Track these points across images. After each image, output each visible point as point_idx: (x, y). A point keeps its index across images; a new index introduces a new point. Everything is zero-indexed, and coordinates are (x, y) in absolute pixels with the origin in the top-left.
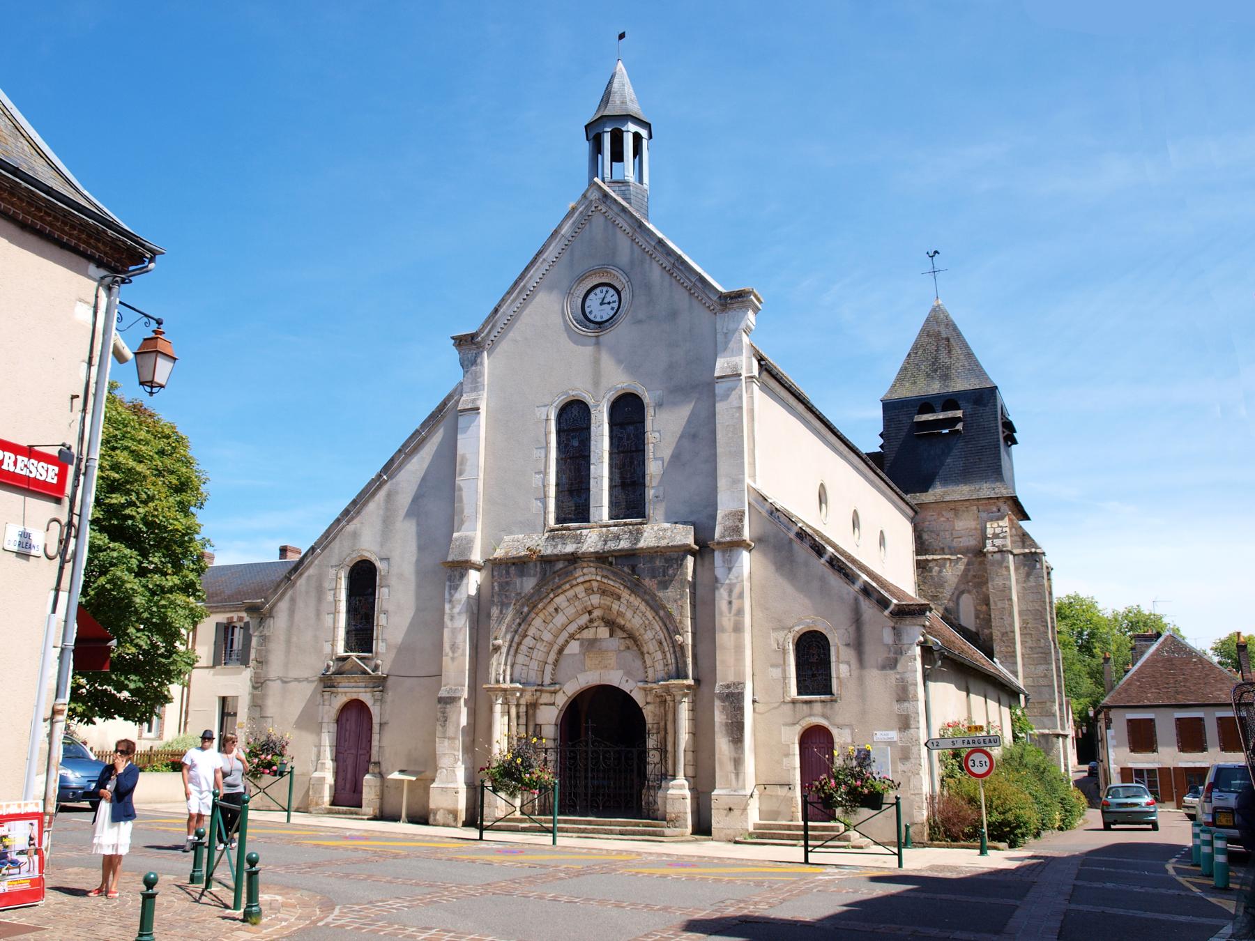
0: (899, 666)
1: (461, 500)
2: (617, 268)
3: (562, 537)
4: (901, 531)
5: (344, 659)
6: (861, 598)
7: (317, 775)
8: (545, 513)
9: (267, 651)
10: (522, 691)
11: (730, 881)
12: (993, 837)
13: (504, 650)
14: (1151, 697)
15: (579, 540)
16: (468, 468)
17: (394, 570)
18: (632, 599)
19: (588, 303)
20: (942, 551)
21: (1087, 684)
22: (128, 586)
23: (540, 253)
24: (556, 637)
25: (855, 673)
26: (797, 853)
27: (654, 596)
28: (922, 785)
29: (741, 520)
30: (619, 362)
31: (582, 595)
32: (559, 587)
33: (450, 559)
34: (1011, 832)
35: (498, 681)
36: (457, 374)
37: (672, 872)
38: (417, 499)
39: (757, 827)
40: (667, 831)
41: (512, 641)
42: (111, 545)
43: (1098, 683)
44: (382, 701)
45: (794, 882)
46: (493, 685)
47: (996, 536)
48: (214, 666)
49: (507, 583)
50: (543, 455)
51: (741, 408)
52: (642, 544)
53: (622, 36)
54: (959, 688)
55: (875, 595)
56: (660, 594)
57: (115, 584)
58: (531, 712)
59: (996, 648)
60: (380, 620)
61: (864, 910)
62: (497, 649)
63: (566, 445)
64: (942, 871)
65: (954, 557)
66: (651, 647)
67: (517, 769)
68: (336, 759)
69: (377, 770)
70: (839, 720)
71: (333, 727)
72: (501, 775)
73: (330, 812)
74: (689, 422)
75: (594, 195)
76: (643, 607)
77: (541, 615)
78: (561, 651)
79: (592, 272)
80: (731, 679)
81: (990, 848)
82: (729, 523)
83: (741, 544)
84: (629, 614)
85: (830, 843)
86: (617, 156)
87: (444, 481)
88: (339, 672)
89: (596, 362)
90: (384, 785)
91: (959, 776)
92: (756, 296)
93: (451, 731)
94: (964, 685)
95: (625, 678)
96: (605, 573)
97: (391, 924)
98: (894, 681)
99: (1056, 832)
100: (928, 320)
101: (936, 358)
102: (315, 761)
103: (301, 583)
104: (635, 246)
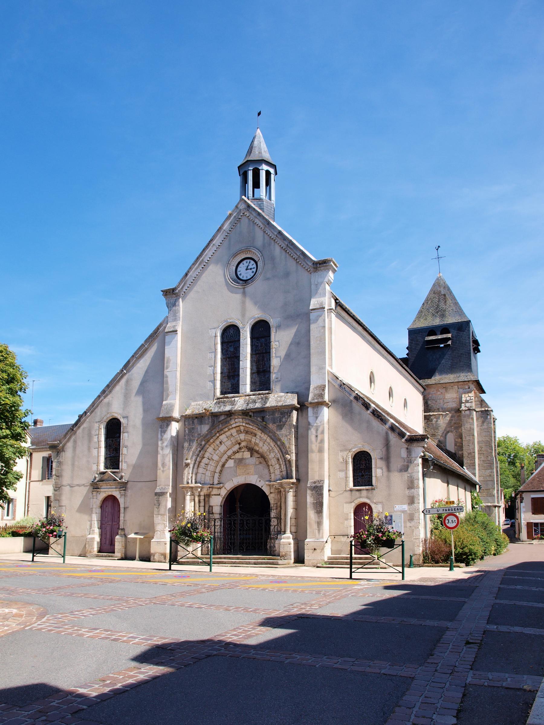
0: (409, 469)
1: (167, 383)
2: (256, 250)
3: (224, 402)
4: (416, 399)
5: (103, 473)
7: (90, 536)
8: (215, 389)
9: (62, 470)
10: (202, 488)
11: (302, 591)
12: (457, 561)
13: (191, 466)
15: (233, 403)
16: (171, 364)
17: (131, 423)
18: (263, 435)
19: (239, 269)
20: (438, 410)
21: (512, 481)
23: (211, 240)
24: (221, 457)
25: (385, 474)
26: (345, 573)
28: (419, 533)
29: (324, 390)
30: (256, 303)
31: (235, 434)
32: (222, 430)
33: (161, 416)
34: (467, 557)
35: (188, 483)
37: (270, 586)
38: (143, 383)
39: (330, 558)
44: (125, 495)
45: (340, 591)
46: (185, 485)
47: (467, 401)
48: (42, 480)
49: (193, 428)
50: (213, 356)
51: (324, 327)
52: (268, 405)
53: (259, 114)
54: (443, 482)
55: (397, 431)
58: (207, 499)
59: (465, 461)
60: (124, 451)
61: (376, 608)
62: (187, 465)
63: (227, 351)
64: (426, 581)
65: (444, 413)
66: (273, 462)
67: (189, 530)
68: (101, 528)
69: (123, 533)
71: (99, 511)
72: (180, 534)
73: (97, 556)
74: (295, 335)
75: (242, 206)
76: (268, 440)
77: (212, 445)
78: (223, 466)
79: (241, 251)
80: (317, 478)
81: (455, 566)
82: (317, 392)
84: (261, 444)
86: (256, 185)
88: (101, 480)
89: (243, 303)
90: (127, 542)
91: (441, 528)
92: (334, 263)
93: (162, 510)
94: (446, 480)
95: (259, 480)
96: (247, 422)
97: (73, 627)
98: (406, 477)
99: (492, 556)
101: (438, 306)
102: (85, 527)
103: (80, 432)
104: (266, 236)
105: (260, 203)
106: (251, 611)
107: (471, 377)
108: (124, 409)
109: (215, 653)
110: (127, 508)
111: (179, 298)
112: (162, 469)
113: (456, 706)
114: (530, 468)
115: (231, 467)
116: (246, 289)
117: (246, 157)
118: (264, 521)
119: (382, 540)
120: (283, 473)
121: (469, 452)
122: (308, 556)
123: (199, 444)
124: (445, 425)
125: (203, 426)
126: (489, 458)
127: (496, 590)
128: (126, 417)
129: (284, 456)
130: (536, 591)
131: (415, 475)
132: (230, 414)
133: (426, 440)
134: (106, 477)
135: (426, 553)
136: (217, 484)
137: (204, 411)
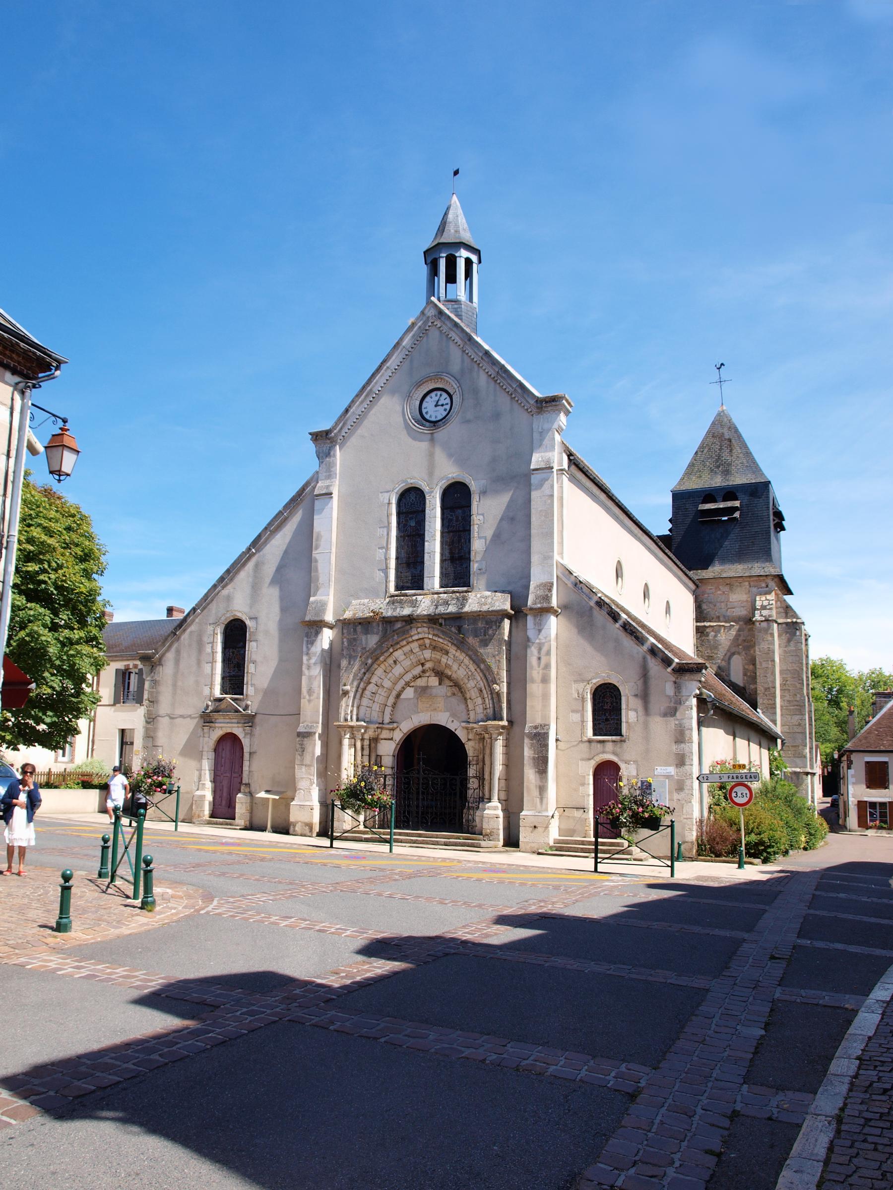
0: (678, 714)
1: (317, 570)
2: (447, 374)
3: (400, 602)
4: (683, 601)
5: (220, 700)
6: (649, 657)
7: (198, 793)
8: (387, 581)
9: (158, 693)
10: (366, 728)
11: (533, 885)
13: (352, 694)
14: (885, 745)
15: (414, 604)
16: (322, 543)
17: (261, 628)
18: (458, 654)
19: (424, 405)
21: (834, 732)
22: (43, 638)
23: (384, 362)
24: (395, 684)
25: (642, 719)
26: (589, 863)
27: (476, 652)
28: (693, 811)
29: (550, 590)
30: (450, 456)
32: (398, 643)
33: (307, 619)
35: (346, 720)
36: (313, 464)
37: (486, 876)
38: (280, 569)
39: (557, 841)
40: (483, 843)
41: (358, 687)
42: (29, 605)
43: (843, 731)
44: (251, 734)
47: (764, 608)
48: (114, 705)
49: (355, 639)
51: (552, 496)
52: (467, 609)
53: (456, 173)
55: (661, 655)
56: (481, 651)
57: (33, 637)
58: (373, 745)
60: (250, 668)
62: (346, 693)
63: (405, 525)
64: (706, 880)
66: (473, 693)
67: (361, 791)
68: (214, 781)
69: (247, 790)
70: (627, 757)
71: (212, 755)
72: (348, 796)
73: (209, 823)
74: (508, 507)
75: (431, 312)
76: (467, 661)
77: (382, 666)
78: (398, 696)
80: (539, 721)
82: (540, 593)
83: (549, 610)
84: (455, 667)
85: (616, 856)
86: (451, 278)
87: (302, 556)
89: (431, 455)
92: (567, 401)
93: (307, 759)
94: (731, 730)
96: (436, 632)
98: (673, 726)
100: (713, 423)
101: (719, 457)
102: (197, 782)
103: (185, 637)
105: (456, 306)
106: (475, 906)
107: (770, 570)
108: (251, 606)
109: (453, 951)
110: (254, 753)
111: (335, 445)
112: (307, 697)
113: (764, 1020)
114: (864, 713)
115: (410, 699)
116: (435, 435)
117: (435, 238)
118: (458, 783)
119: (642, 817)
120: (488, 711)
121: (766, 686)
122: (524, 836)
123: (363, 663)
124: (729, 644)
125: (369, 636)
126: (798, 697)
127: (808, 897)
128: (254, 618)
129: (489, 686)
130: (867, 902)
131: (686, 722)
132: (410, 620)
133: (704, 671)
134: (223, 705)
135: (702, 840)
136: (388, 724)
137: (372, 614)
